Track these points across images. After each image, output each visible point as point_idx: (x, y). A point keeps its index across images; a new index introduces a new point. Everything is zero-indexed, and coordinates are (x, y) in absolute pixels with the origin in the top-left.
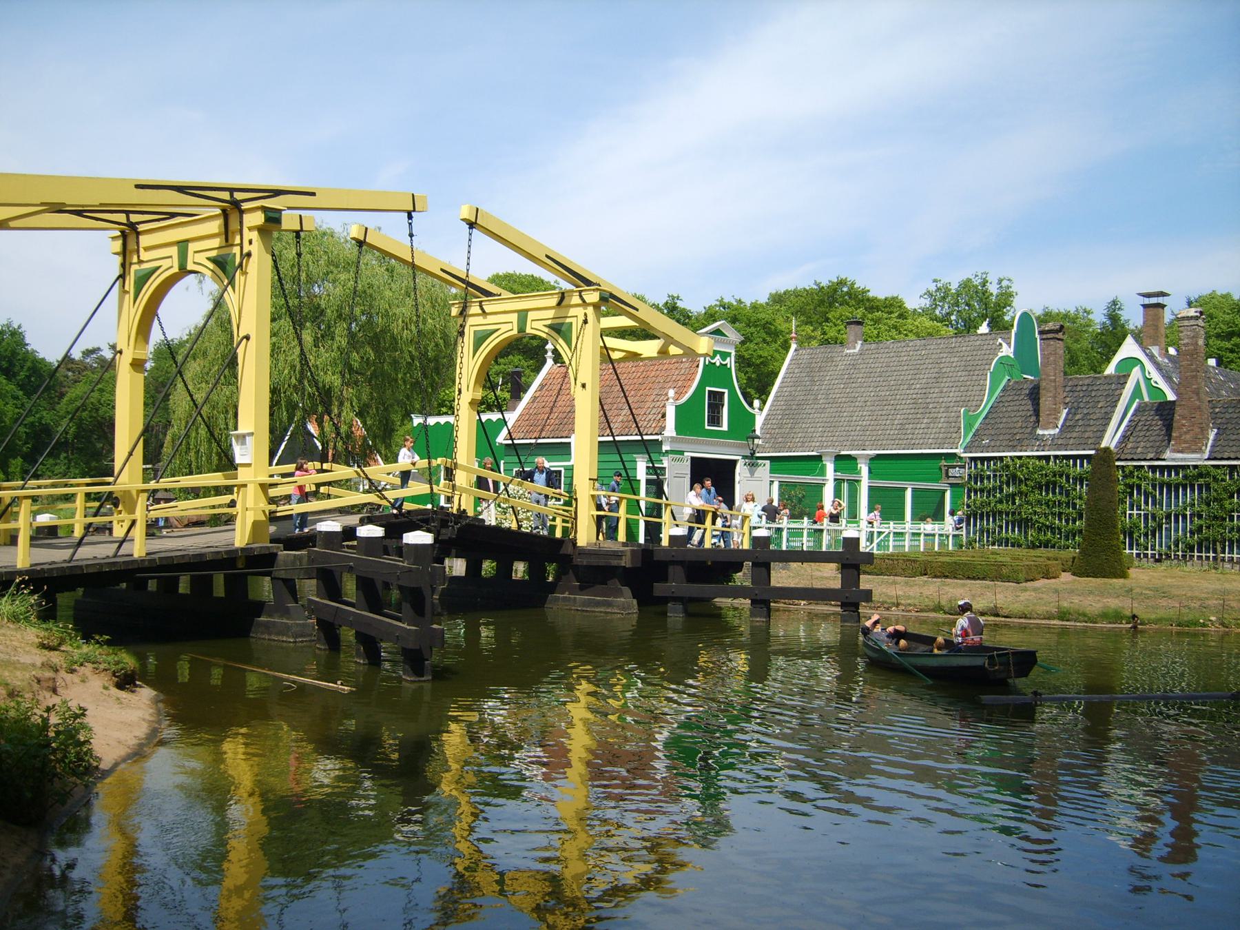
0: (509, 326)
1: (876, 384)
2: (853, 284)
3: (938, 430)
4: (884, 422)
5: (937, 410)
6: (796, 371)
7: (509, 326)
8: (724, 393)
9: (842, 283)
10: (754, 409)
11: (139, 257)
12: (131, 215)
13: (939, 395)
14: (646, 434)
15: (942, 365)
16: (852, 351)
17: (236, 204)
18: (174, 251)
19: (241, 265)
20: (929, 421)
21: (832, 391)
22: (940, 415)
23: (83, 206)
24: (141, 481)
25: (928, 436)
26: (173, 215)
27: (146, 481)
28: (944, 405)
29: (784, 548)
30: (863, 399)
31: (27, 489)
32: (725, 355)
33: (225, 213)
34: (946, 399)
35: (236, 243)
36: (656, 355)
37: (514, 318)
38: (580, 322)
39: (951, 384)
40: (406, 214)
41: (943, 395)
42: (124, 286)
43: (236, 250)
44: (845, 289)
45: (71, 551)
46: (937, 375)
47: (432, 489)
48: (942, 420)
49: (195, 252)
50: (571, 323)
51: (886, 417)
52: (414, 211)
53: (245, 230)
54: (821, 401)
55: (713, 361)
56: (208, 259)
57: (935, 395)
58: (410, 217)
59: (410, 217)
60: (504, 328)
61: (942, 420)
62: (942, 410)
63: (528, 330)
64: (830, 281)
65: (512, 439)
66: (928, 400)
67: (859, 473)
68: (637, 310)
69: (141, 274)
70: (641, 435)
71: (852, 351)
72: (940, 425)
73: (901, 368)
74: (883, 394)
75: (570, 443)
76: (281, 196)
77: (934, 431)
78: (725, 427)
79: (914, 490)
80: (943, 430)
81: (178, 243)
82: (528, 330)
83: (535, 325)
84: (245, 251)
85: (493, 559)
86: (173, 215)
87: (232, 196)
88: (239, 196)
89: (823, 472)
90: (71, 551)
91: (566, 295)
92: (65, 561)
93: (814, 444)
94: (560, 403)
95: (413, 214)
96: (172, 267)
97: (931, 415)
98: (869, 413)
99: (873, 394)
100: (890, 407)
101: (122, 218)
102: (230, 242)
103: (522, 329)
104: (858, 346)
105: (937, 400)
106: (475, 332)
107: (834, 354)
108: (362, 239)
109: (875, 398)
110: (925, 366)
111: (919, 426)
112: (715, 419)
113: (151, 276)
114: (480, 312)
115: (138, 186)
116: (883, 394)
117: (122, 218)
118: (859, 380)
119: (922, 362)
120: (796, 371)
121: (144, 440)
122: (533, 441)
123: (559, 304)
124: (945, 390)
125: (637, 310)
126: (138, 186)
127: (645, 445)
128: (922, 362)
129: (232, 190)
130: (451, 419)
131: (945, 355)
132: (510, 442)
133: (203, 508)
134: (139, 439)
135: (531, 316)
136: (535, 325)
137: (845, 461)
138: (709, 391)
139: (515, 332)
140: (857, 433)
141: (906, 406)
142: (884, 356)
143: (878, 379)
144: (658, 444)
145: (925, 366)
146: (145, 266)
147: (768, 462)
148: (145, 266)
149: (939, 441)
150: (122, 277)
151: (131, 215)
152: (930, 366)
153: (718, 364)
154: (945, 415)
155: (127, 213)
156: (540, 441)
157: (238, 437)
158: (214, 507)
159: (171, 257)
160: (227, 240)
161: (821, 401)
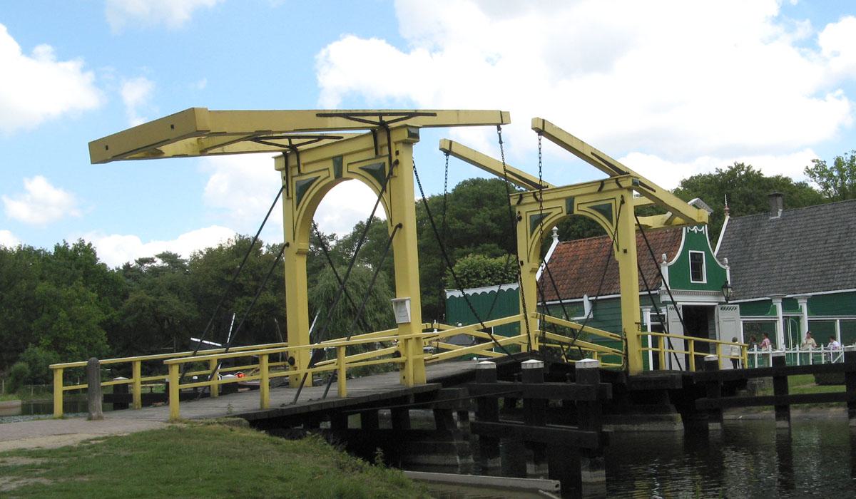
0: (559, 210)
2: (749, 168)
6: (732, 236)
7: (559, 210)
8: (702, 254)
9: (740, 167)
10: (724, 265)
11: (299, 171)
12: (292, 140)
14: (564, 299)
15: (850, 223)
16: (775, 218)
17: (383, 125)
18: (330, 165)
19: (391, 173)
20: (845, 267)
21: (763, 250)
23: (281, 132)
24: (309, 342)
26: (320, 138)
27: (312, 342)
29: (798, 364)
30: (789, 254)
31: (198, 355)
32: (700, 225)
33: (374, 133)
35: (384, 154)
36: (662, 226)
37: (563, 204)
38: (618, 203)
40: (496, 127)
42: (288, 195)
43: (386, 160)
44: (743, 173)
45: (324, 388)
47: (544, 333)
49: (348, 164)
50: (611, 204)
51: (809, 267)
52: (502, 123)
53: (393, 145)
54: (755, 259)
55: (692, 230)
56: (361, 168)
57: (846, 247)
58: (499, 129)
59: (499, 129)
60: (555, 212)
63: (576, 212)
64: (729, 167)
67: (801, 310)
68: (655, 191)
69: (302, 184)
70: (649, 291)
71: (775, 218)
73: (817, 228)
74: (805, 249)
76: (413, 118)
78: (705, 281)
79: (695, 342)
81: (334, 158)
82: (576, 212)
83: (581, 207)
84: (394, 160)
86: (320, 138)
87: (381, 119)
88: (386, 119)
89: (774, 312)
90: (324, 388)
91: (605, 182)
92: (291, 403)
93: (753, 293)
95: (501, 126)
96: (329, 176)
97: (846, 263)
98: (796, 265)
99: (796, 250)
100: (812, 259)
101: (286, 142)
102: (379, 154)
103: (570, 211)
104: (780, 214)
106: (530, 216)
107: (762, 221)
108: (448, 149)
109: (799, 253)
110: (836, 225)
111: (837, 272)
112: (697, 275)
113: (311, 184)
114: (534, 200)
115: (318, 115)
116: (805, 249)
117: (376, 119)
118: (784, 240)
119: (833, 222)
120: (732, 236)
123: (600, 190)
125: (655, 191)
126: (318, 115)
127: (652, 298)
128: (833, 222)
129: (381, 114)
130: (514, 286)
131: (851, 215)
133: (362, 361)
135: (577, 201)
136: (581, 207)
137: (790, 305)
138: (702, 254)
139: (564, 214)
140: (786, 281)
141: (824, 257)
142: (802, 219)
143: (799, 238)
144: (658, 296)
145: (836, 225)
146: (305, 178)
147: (738, 306)
148: (305, 178)
150: (285, 187)
151: (292, 140)
152: (840, 225)
153: (696, 232)
155: (290, 138)
156: (599, 298)
157: (397, 303)
158: (367, 360)
159: (328, 169)
160: (377, 153)
161: (755, 259)
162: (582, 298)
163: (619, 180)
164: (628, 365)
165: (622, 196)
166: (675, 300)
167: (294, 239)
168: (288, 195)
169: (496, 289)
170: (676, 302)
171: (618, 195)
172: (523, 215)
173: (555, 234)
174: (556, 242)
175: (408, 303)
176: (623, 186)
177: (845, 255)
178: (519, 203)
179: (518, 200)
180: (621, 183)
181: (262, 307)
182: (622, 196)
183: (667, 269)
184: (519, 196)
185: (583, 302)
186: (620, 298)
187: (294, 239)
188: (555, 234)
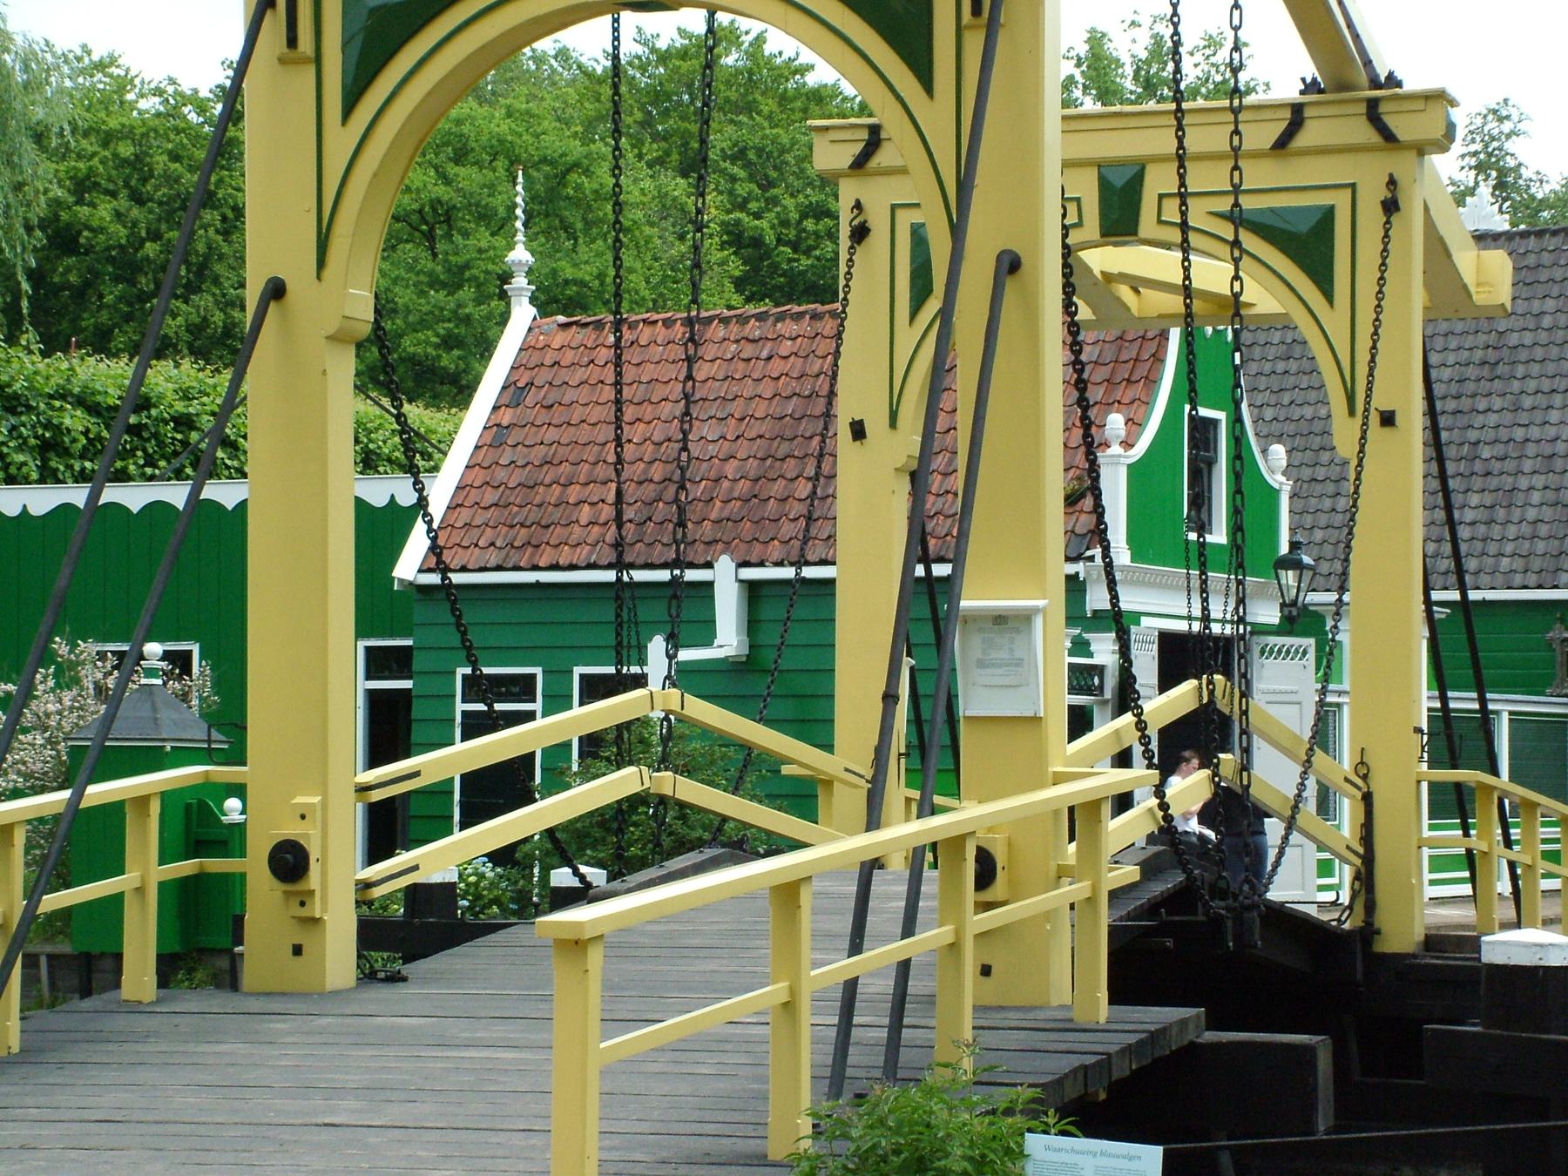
1: (1275, 383)
3: (1525, 529)
4: (1327, 503)
5: (1510, 465)
13: (1507, 418)
20: (1488, 499)
22: (1523, 483)
25: (1492, 548)
28: (1531, 449)
34: (1535, 432)
39: (1546, 385)
41: (1523, 418)
42: (292, 42)
46: (1492, 355)
48: (1536, 497)
57: (1493, 419)
61: (1536, 497)
62: (1528, 465)
65: (444, 570)
66: (1473, 435)
72: (1531, 514)
75: (709, 585)
77: (1512, 531)
80: (1543, 530)
85: (1104, 1101)
91: (1308, 113)
94: (709, 430)
97: (1493, 482)
105: (1504, 434)
121: (1102, 1060)
122: (788, 573)
123: (1282, 143)
124: (1527, 402)
132: (434, 579)
134: (1277, 863)
143: (1280, 367)
149: (1537, 564)
154: (1539, 481)
162: (709, 565)
163: (1383, 108)
164: (1370, 907)
165: (1392, 182)
166: (1124, 605)
167: (321, 263)
168: (292, 42)
169: (176, 494)
170: (1136, 616)
171: (1370, 176)
172: (878, 222)
173: (520, 281)
174: (522, 314)
175: (1038, 623)
176: (1402, 135)
177: (1486, 452)
178: (860, 163)
179: (857, 148)
180: (1391, 121)
181: (1463, 702)
182: (1392, 182)
183: (1123, 474)
184: (865, 135)
185: (709, 585)
186: (831, 582)
187: (321, 263)
188: (520, 281)
